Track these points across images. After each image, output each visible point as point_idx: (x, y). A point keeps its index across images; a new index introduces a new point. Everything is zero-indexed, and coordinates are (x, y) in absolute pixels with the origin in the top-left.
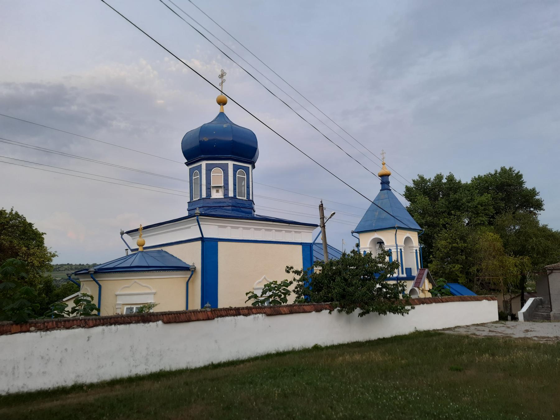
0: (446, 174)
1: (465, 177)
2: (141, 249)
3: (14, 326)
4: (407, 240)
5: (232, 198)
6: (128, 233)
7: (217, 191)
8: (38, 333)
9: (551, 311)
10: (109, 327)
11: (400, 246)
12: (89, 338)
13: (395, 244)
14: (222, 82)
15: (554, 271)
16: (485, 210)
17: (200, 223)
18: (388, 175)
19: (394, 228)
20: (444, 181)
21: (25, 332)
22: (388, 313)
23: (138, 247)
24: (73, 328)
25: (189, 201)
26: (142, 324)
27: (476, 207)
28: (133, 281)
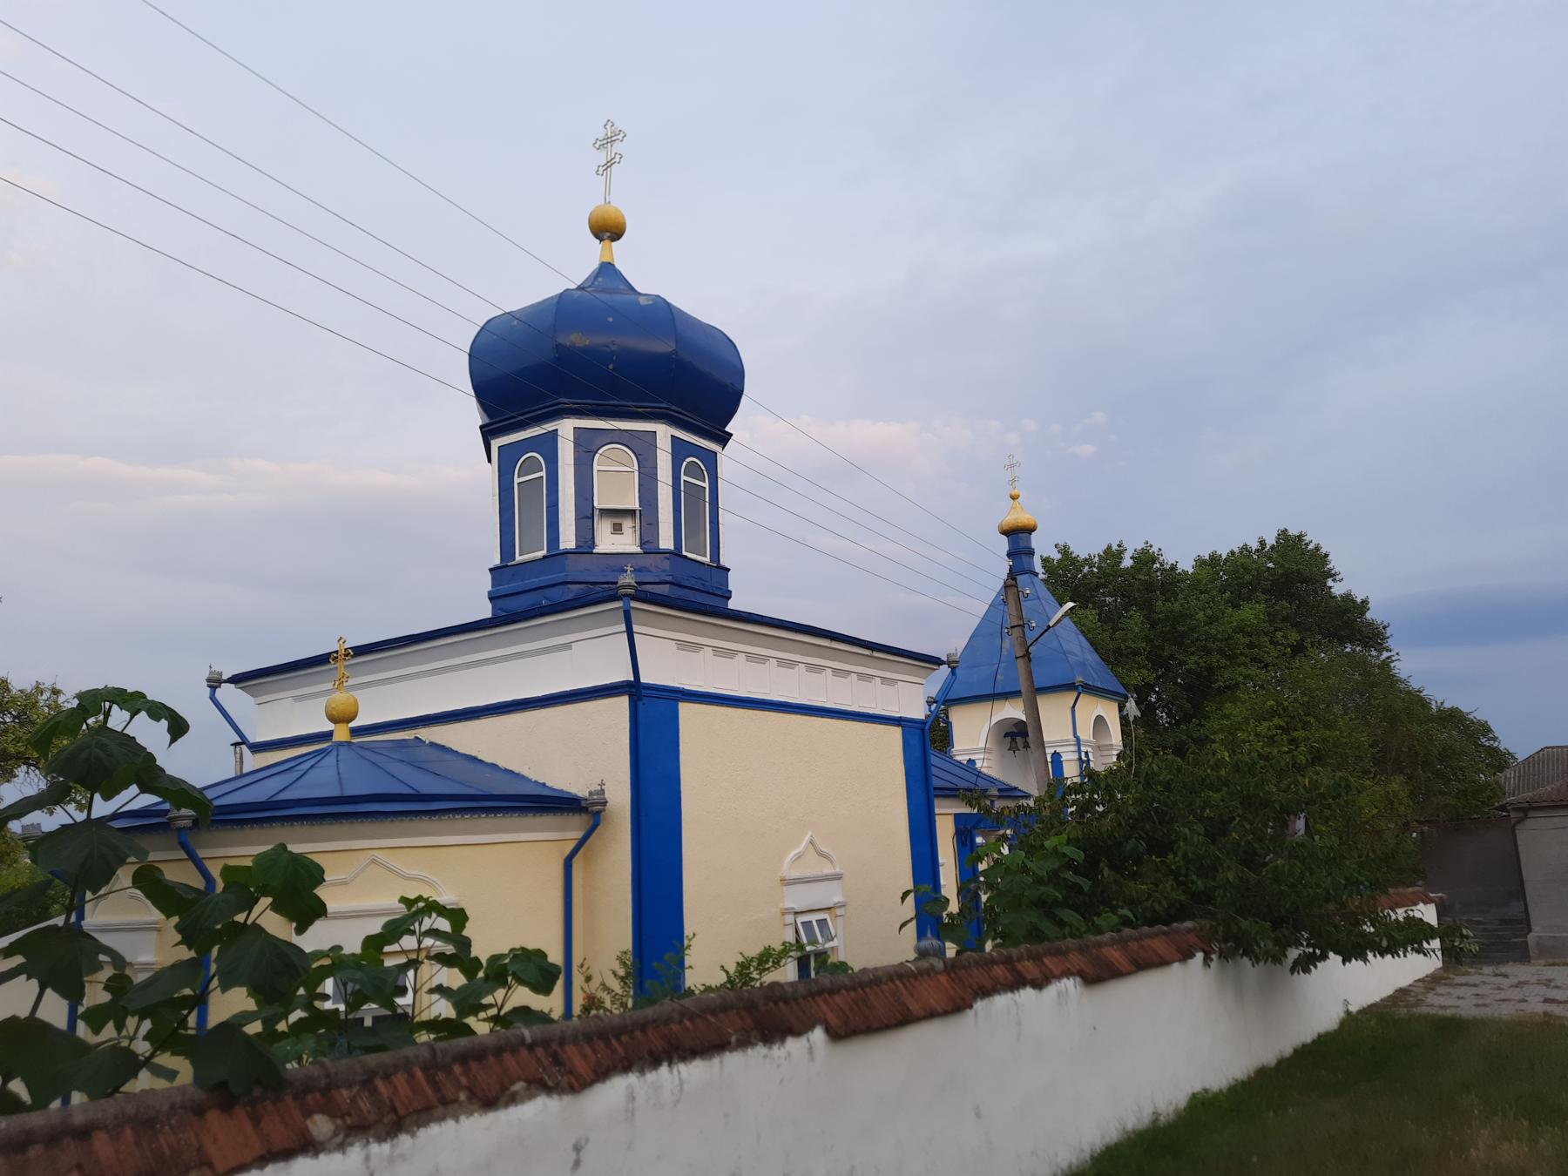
0: (1133, 546)
1: (1182, 555)
2: (341, 734)
3: (213, 1116)
4: (1100, 721)
5: (670, 553)
6: (236, 680)
7: (617, 529)
8: (355, 1153)
9: (1530, 930)
10: (651, 1076)
11: (1087, 743)
12: (577, 1149)
13: (1071, 737)
14: (609, 165)
15: (1531, 814)
16: (1250, 646)
17: (636, 628)
18: (1030, 530)
19: (1070, 687)
20: (1127, 563)
21: (286, 1154)
22: (1370, 956)
23: (329, 726)
24: (513, 1100)
25: (497, 561)
26: (761, 1050)
27: (1230, 637)
28: (364, 858)
